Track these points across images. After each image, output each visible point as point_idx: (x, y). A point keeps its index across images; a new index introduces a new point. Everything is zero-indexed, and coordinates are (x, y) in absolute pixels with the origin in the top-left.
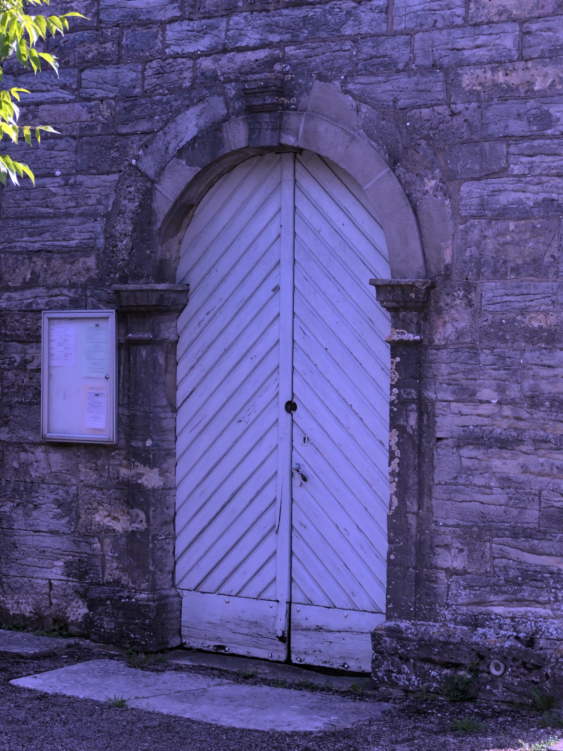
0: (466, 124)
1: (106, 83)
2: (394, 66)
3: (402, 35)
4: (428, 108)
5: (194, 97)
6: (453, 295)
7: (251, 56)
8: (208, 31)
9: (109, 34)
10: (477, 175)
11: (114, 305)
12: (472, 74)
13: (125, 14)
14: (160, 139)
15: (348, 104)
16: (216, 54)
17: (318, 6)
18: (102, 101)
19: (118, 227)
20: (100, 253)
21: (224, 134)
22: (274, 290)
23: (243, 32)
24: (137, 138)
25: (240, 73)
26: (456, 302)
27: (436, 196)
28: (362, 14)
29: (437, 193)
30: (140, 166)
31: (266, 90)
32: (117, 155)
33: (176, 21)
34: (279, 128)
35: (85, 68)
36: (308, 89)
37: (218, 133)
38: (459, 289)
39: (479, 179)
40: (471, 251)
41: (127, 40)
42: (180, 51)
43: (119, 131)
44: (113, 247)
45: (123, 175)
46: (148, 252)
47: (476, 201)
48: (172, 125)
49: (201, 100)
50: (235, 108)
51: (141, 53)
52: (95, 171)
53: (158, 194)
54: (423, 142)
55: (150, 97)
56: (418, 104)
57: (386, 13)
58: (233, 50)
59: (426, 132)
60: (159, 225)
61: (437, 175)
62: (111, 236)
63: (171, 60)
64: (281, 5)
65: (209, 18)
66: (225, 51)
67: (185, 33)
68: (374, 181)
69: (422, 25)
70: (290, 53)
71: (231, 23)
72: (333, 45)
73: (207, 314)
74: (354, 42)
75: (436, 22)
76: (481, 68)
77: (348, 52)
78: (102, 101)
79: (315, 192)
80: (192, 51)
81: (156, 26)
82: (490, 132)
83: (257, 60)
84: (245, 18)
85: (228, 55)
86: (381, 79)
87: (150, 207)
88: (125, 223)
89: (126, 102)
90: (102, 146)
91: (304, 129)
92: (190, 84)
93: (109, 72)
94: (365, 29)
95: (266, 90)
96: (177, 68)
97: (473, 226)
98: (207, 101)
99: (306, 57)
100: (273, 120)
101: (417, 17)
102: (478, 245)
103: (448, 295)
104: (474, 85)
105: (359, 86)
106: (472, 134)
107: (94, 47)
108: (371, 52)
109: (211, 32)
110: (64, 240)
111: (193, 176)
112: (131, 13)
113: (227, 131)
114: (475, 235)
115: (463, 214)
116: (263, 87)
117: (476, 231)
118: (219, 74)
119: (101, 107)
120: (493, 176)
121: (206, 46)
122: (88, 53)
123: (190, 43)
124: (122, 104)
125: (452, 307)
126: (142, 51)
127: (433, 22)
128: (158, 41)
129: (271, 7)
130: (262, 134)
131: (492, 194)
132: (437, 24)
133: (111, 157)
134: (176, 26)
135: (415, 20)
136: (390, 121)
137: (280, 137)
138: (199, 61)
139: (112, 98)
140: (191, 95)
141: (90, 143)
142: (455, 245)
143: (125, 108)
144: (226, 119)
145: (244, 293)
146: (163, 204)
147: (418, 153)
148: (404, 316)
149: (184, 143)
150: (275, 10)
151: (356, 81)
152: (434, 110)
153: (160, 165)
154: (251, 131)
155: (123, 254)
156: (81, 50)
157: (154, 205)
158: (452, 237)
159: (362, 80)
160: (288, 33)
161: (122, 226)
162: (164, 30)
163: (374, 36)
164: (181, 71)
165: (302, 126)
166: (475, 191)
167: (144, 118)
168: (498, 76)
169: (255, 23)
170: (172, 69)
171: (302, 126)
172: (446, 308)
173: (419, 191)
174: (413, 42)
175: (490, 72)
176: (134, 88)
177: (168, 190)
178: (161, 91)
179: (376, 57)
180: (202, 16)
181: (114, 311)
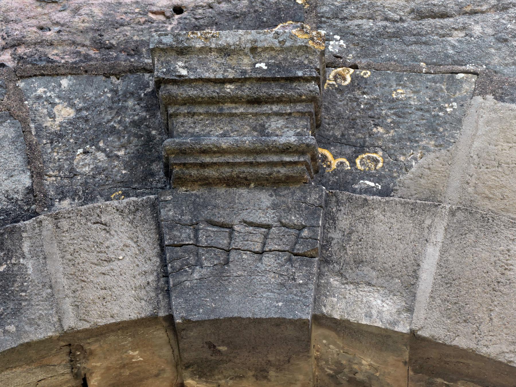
21: (30, 265)
31: (277, 91)
36: (441, 128)
50: (73, 173)
83: (178, 10)
91: (442, 264)
95: (277, 91)
100: (295, 219)
110: (495, 180)
113: (41, 255)
130: (235, 270)
137: (321, 291)
154: (168, 266)
165: (431, 257)
171: (431, 257)
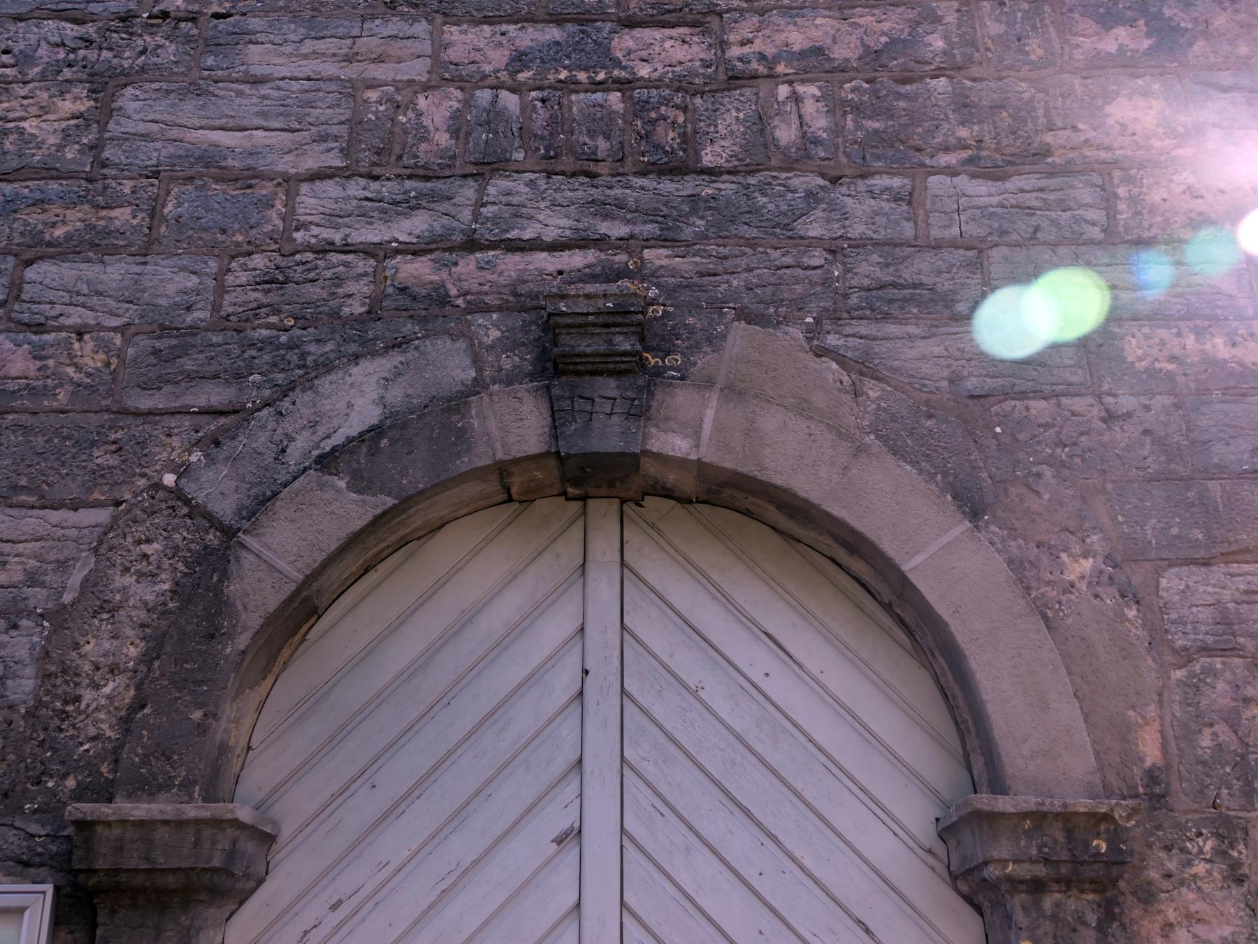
0: (1148, 440)
1: (99, 294)
2: (946, 307)
3: (957, 248)
4: (1045, 399)
5: (376, 338)
6: (1183, 850)
7: (544, 261)
8: (424, 203)
9: (127, 191)
10: (1202, 553)
11: (43, 871)
12: (1147, 337)
13: (181, 152)
14: (263, 427)
15: (830, 377)
16: (444, 250)
17: (725, 177)
18: (80, 335)
19: (88, 648)
20: (15, 717)
21: (476, 423)
22: (559, 841)
23: (524, 210)
24: (187, 422)
25: (515, 294)
26: (1194, 870)
27: (1097, 596)
28: (849, 200)
29: (1099, 589)
30: (190, 489)
31: (619, 320)
32: (116, 463)
33: (331, 177)
34: (639, 413)
35: (41, 258)
36: (714, 340)
37: (455, 418)
38: (1200, 834)
39: (1207, 563)
40: (1215, 735)
41: (178, 205)
42: (337, 237)
43: (129, 403)
44: (66, 702)
45: (129, 511)
46: (197, 715)
47: (1205, 614)
48: (302, 398)
49: (400, 344)
50: (500, 369)
51: (220, 237)
52: (32, 499)
53: (247, 559)
54: (1048, 472)
55: (239, 331)
56: (1017, 389)
57: (909, 203)
58: (493, 246)
59: (1049, 451)
60: (243, 641)
61: (1096, 547)
62: (64, 672)
63: (309, 256)
64: (628, 167)
65: (427, 178)
66: (471, 245)
67: (355, 203)
68: (934, 548)
69: (1003, 233)
70: (658, 263)
71: (491, 190)
72: (774, 254)
73: (334, 907)
74: (831, 252)
75: (1037, 229)
76: (1170, 327)
77: (819, 271)
78: (80, 335)
79: (685, 593)
80: (376, 239)
81: (268, 184)
82: (1216, 460)
83: (560, 273)
84: (531, 184)
85: (478, 255)
86: (912, 329)
87: (218, 593)
88: (115, 637)
89: (160, 337)
90: (65, 438)
92: (364, 309)
93: (115, 273)
94: (858, 230)
95: (619, 320)
96: (328, 274)
97: (1209, 671)
98: (417, 348)
99: (702, 275)
100: (630, 394)
101: (991, 216)
102: (1232, 719)
103: (1168, 849)
104: (1157, 360)
105: (852, 342)
106: (1170, 461)
107: (72, 215)
108: (879, 274)
109: (432, 206)
111: (369, 517)
112: (198, 153)
114: (1219, 695)
115: (1180, 643)
116: (611, 313)
117: (1221, 686)
118: (453, 291)
119: (76, 345)
120: (1240, 557)
121: (417, 232)
122: (54, 225)
123: (371, 224)
124: (145, 342)
125: (1182, 883)
126: (224, 231)
127: (1031, 230)
128: (272, 214)
129: (603, 169)
130: (595, 424)
131: (1245, 598)
132: (1039, 235)
133: (90, 465)
134: (330, 188)
135: (985, 221)
136: (946, 421)
138: (391, 263)
139: (115, 329)
140: (365, 335)
141: (26, 429)
142: (1168, 718)
143: (156, 352)
144: (478, 386)
145: (462, 847)
146: (257, 589)
147: (1037, 493)
148: (1057, 905)
149: (338, 439)
150: (613, 176)
151: (848, 330)
152: (1059, 405)
153: (253, 491)
155: (96, 722)
156: (34, 218)
157: (233, 589)
158: (1156, 697)
159: (862, 328)
160: (652, 221)
161: (107, 645)
162: (291, 195)
163: (885, 244)
164: (338, 280)
165: (709, 415)
166: (1202, 589)
167: (215, 377)
168: (1214, 346)
169: (557, 196)
170: (312, 275)
172: (1166, 885)
173: (1048, 583)
174: (985, 263)
175: (1193, 337)
176: (188, 309)
177: (284, 549)
178: (273, 319)
179: (894, 285)
180: (408, 172)
181: (49, 888)
